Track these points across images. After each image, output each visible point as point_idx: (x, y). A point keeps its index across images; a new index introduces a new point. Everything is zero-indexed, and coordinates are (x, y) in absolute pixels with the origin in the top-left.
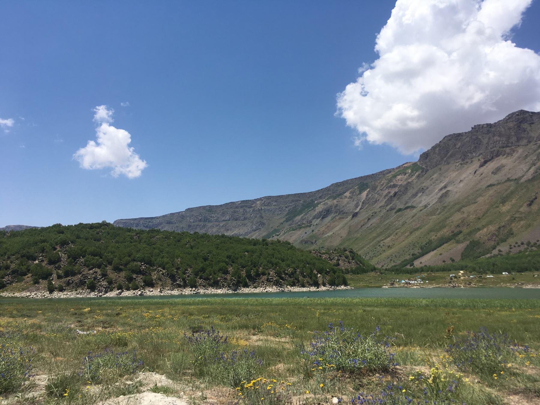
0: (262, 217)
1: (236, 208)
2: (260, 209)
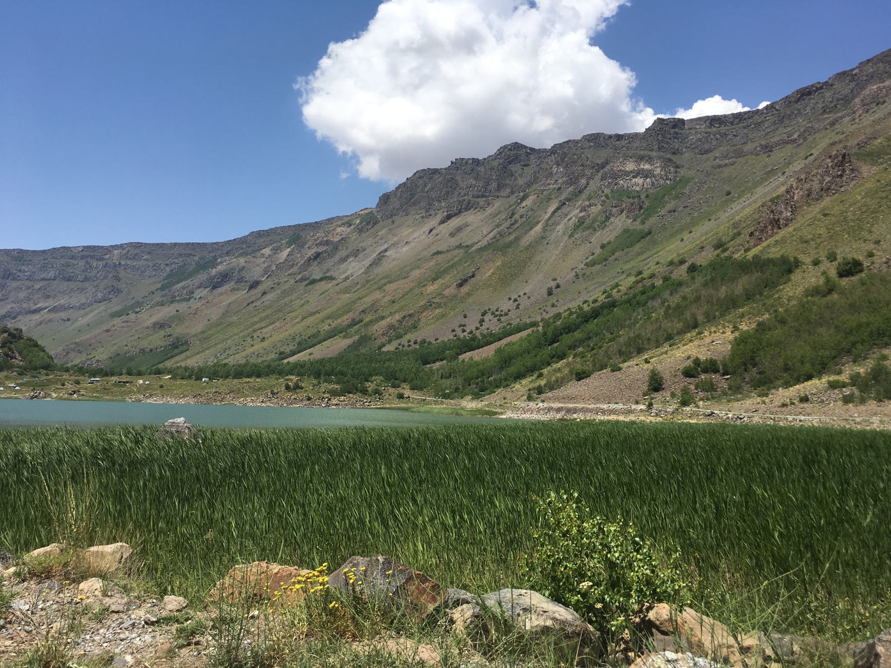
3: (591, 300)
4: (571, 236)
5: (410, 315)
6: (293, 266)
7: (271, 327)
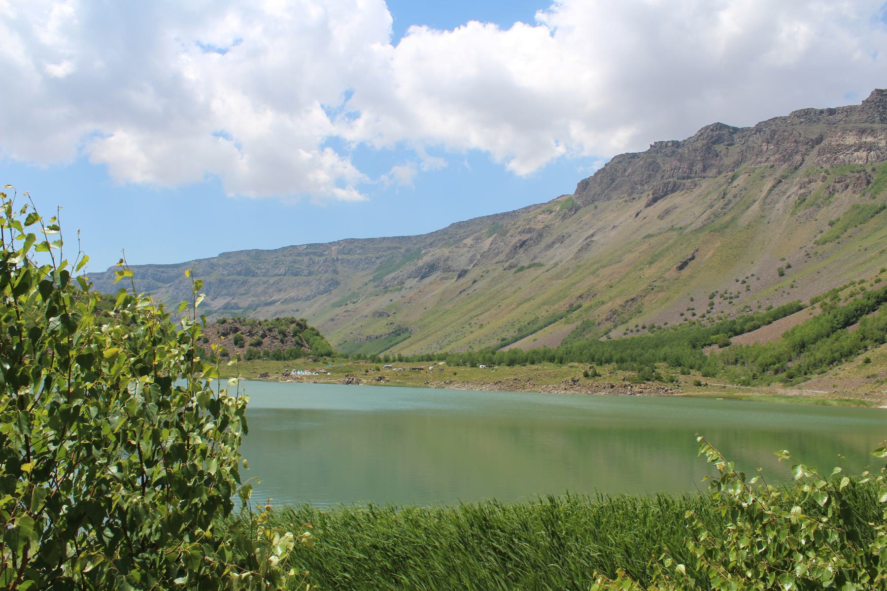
0: (335, 272)
1: (298, 256)
2: (335, 258)
3: (857, 280)
4: (793, 214)
5: (632, 300)
6: (497, 254)
7: (487, 314)
